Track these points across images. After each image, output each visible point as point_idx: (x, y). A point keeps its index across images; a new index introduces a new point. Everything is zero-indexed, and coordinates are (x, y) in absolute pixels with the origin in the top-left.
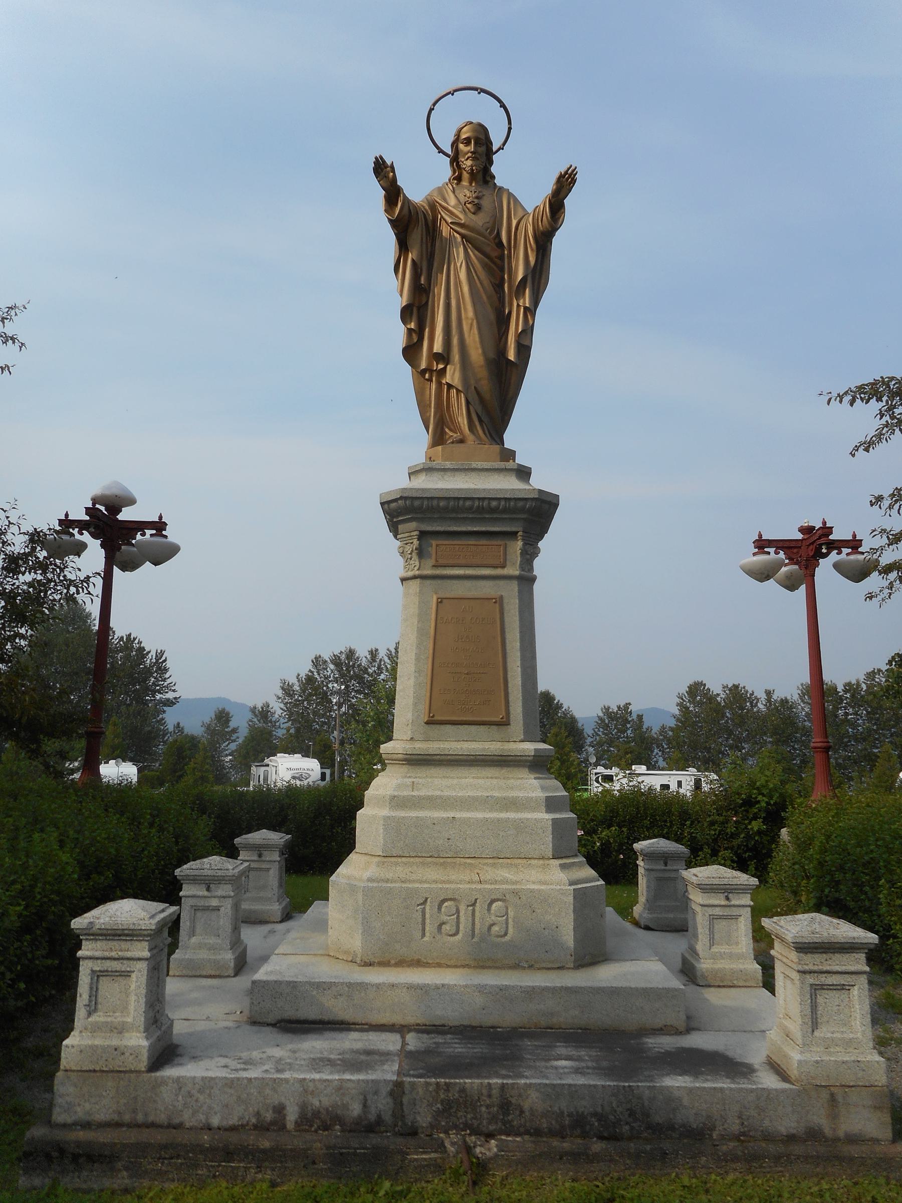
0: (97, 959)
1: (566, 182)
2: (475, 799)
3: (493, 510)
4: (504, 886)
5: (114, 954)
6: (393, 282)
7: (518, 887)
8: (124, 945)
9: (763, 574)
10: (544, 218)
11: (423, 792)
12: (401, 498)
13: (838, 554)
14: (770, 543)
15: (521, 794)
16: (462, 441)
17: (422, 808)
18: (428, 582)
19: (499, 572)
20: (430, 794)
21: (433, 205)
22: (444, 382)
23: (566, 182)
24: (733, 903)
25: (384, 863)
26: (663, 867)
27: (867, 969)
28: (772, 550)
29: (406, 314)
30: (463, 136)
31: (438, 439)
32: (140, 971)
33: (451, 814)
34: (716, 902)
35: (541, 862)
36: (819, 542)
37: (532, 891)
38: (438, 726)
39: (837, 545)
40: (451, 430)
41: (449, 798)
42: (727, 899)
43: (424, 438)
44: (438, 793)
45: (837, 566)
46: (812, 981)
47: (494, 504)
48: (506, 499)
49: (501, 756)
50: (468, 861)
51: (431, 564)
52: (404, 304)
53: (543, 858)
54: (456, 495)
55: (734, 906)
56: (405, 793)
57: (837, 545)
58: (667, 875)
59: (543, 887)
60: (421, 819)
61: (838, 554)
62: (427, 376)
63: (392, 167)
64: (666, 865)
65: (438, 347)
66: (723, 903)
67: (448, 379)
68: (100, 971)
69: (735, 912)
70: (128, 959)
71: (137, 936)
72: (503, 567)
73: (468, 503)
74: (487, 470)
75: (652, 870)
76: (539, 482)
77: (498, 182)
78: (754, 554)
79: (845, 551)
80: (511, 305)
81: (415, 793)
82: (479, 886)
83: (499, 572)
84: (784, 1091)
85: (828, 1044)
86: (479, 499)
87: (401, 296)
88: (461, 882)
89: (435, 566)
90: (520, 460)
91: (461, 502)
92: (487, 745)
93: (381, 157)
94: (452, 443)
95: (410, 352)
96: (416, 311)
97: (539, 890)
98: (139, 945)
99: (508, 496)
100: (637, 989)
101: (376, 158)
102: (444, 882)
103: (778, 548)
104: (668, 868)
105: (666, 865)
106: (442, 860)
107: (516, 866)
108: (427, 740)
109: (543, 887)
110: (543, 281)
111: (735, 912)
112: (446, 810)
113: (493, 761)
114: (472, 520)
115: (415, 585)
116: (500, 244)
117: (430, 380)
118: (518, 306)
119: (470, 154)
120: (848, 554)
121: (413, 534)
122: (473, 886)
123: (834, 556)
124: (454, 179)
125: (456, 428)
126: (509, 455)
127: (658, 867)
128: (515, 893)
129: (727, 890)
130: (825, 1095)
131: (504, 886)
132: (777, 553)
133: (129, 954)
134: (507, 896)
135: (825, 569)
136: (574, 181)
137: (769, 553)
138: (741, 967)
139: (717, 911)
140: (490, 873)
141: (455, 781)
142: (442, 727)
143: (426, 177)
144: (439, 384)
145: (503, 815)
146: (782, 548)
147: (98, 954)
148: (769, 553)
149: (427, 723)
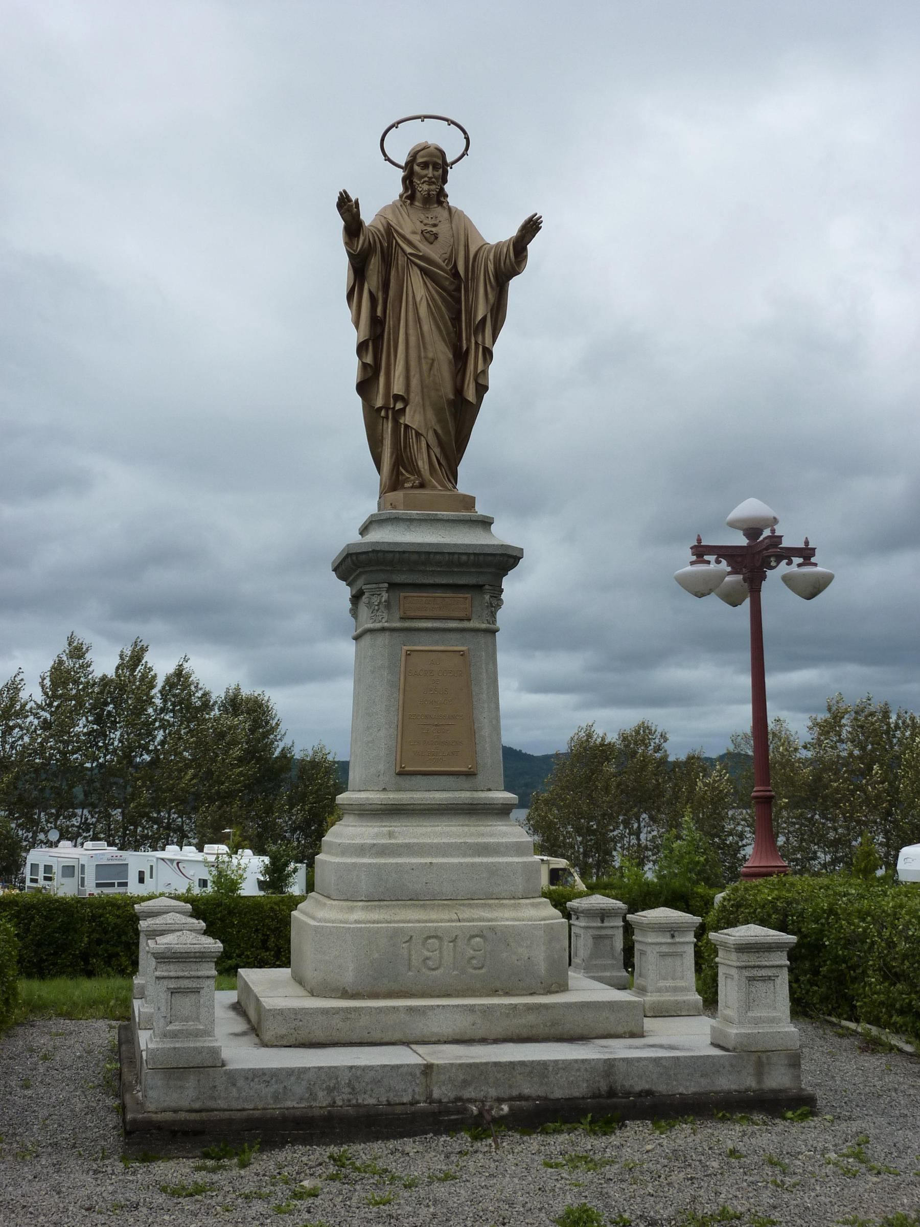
0: (171, 978)
1: (531, 227)
2: (449, 845)
3: (461, 564)
4: (481, 924)
5: (186, 974)
6: (346, 313)
7: (494, 923)
8: (194, 967)
9: (699, 589)
10: (508, 261)
11: (400, 841)
12: (373, 551)
13: (788, 564)
14: (711, 550)
15: (491, 840)
16: (422, 486)
17: (400, 855)
18: (396, 634)
19: (465, 624)
20: (407, 841)
21: (389, 229)
22: (402, 421)
23: (531, 227)
24: (677, 940)
25: (367, 906)
26: (600, 925)
27: (788, 963)
28: (712, 558)
29: (361, 348)
30: (420, 160)
31: (393, 484)
32: (208, 987)
33: (428, 860)
34: (663, 940)
35: (513, 901)
36: (765, 553)
37: (507, 927)
38: (409, 777)
39: (788, 554)
40: (407, 471)
41: (424, 845)
42: (673, 936)
43: (373, 478)
44: (415, 841)
45: (787, 580)
46: (747, 974)
47: (464, 558)
48: (475, 554)
49: (471, 804)
50: (446, 902)
51: (398, 616)
52: (361, 340)
53: (514, 898)
54: (427, 550)
55: (679, 943)
56: (383, 841)
57: (788, 554)
58: (604, 932)
59: (516, 923)
60: (401, 865)
61: (788, 564)
62: (383, 413)
63: (357, 202)
64: (603, 922)
65: (398, 388)
66: (669, 940)
67: (407, 419)
68: (175, 988)
69: (680, 949)
70: (198, 977)
71: (206, 957)
72: (469, 620)
73: (438, 557)
74: (448, 521)
75: (590, 928)
76: (503, 534)
77: (452, 201)
78: (692, 563)
79: (797, 560)
80: (469, 340)
81: (393, 841)
82: (458, 924)
83: (465, 624)
84: (722, 1056)
85: (757, 1021)
86: (449, 553)
87: (357, 327)
88: (441, 921)
89: (402, 619)
90: (481, 509)
91: (432, 556)
92: (457, 795)
93: (345, 192)
94: (412, 487)
95: (364, 387)
96: (374, 346)
97: (513, 926)
98: (206, 965)
99: (477, 551)
100: (603, 1002)
101: (341, 193)
102: (426, 921)
103: (719, 556)
104: (606, 924)
105: (603, 922)
106: (422, 903)
107: (490, 906)
108: (399, 790)
109: (516, 923)
110: (500, 317)
111: (680, 949)
112: (422, 856)
113: (463, 809)
114: (440, 573)
115: (383, 640)
116: (456, 274)
117: (387, 417)
118: (476, 343)
119: (426, 179)
120: (799, 565)
121: (381, 585)
122: (454, 924)
123: (783, 568)
124: (407, 198)
125: (416, 471)
126: (468, 502)
127: (595, 924)
128: (492, 929)
129: (672, 930)
130: (754, 1057)
131: (481, 924)
132: (718, 562)
133: (200, 973)
134: (485, 932)
135: (775, 576)
136: (538, 229)
137: (708, 562)
138: (685, 998)
139: (665, 949)
140: (467, 913)
141: (429, 829)
142: (413, 778)
143: (380, 195)
144: (396, 423)
145: (477, 860)
146: (725, 556)
147: (172, 974)
148: (708, 562)
149: (400, 774)
